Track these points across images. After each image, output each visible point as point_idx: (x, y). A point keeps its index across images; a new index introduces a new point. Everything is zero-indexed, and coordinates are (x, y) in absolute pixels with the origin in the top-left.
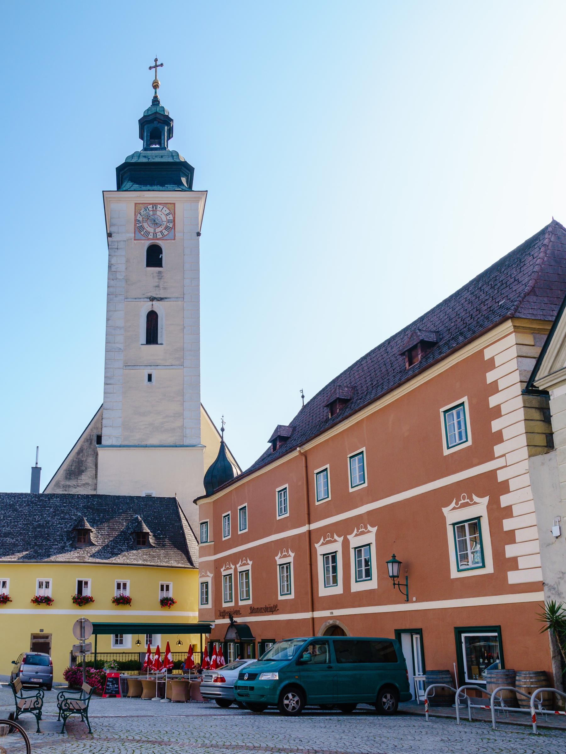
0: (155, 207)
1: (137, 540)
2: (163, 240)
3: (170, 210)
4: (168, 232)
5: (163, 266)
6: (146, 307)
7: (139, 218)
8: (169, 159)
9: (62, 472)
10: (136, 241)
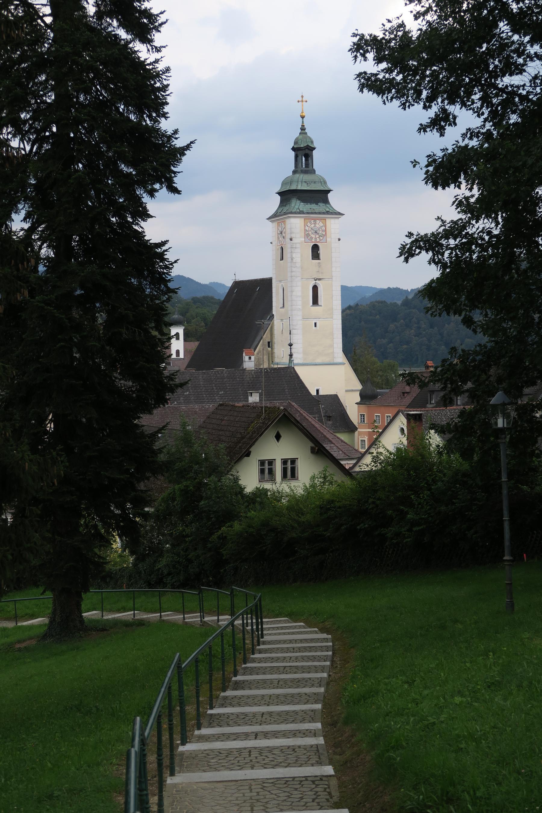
6: (312, 283)
7: (307, 228)
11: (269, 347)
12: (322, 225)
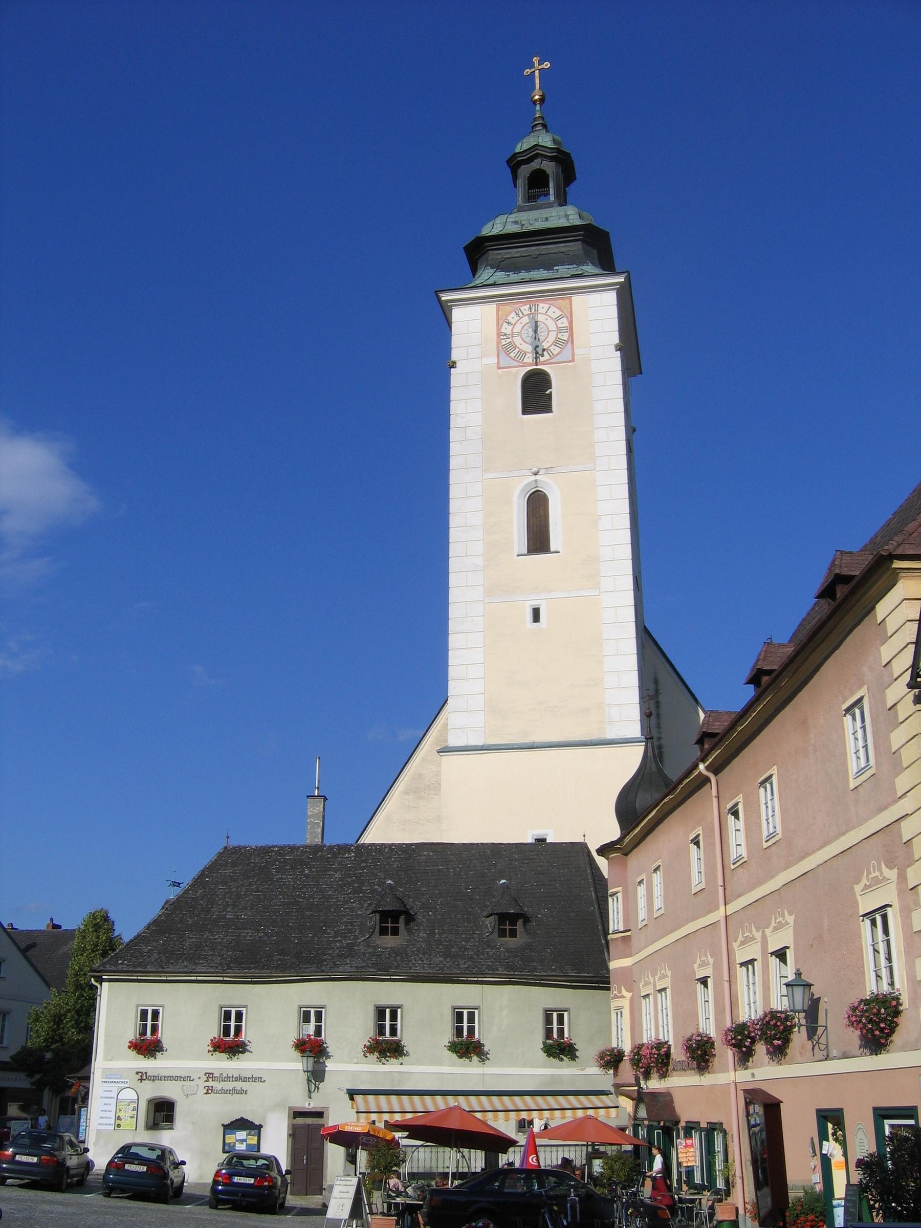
0: (533, 308)
1: (499, 929)
2: (552, 363)
3: (562, 311)
4: (560, 349)
5: (553, 410)
7: (506, 329)
8: (561, 221)
12: (558, 313)
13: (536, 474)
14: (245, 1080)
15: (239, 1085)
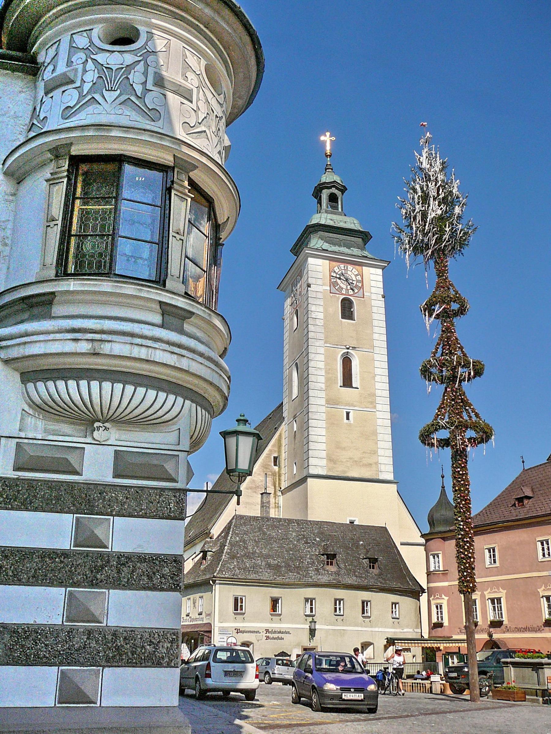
8: (352, 225)
9: (258, 465)
10: (331, 294)
11: (275, 465)
13: (348, 349)
14: (283, 633)
15: (280, 635)
